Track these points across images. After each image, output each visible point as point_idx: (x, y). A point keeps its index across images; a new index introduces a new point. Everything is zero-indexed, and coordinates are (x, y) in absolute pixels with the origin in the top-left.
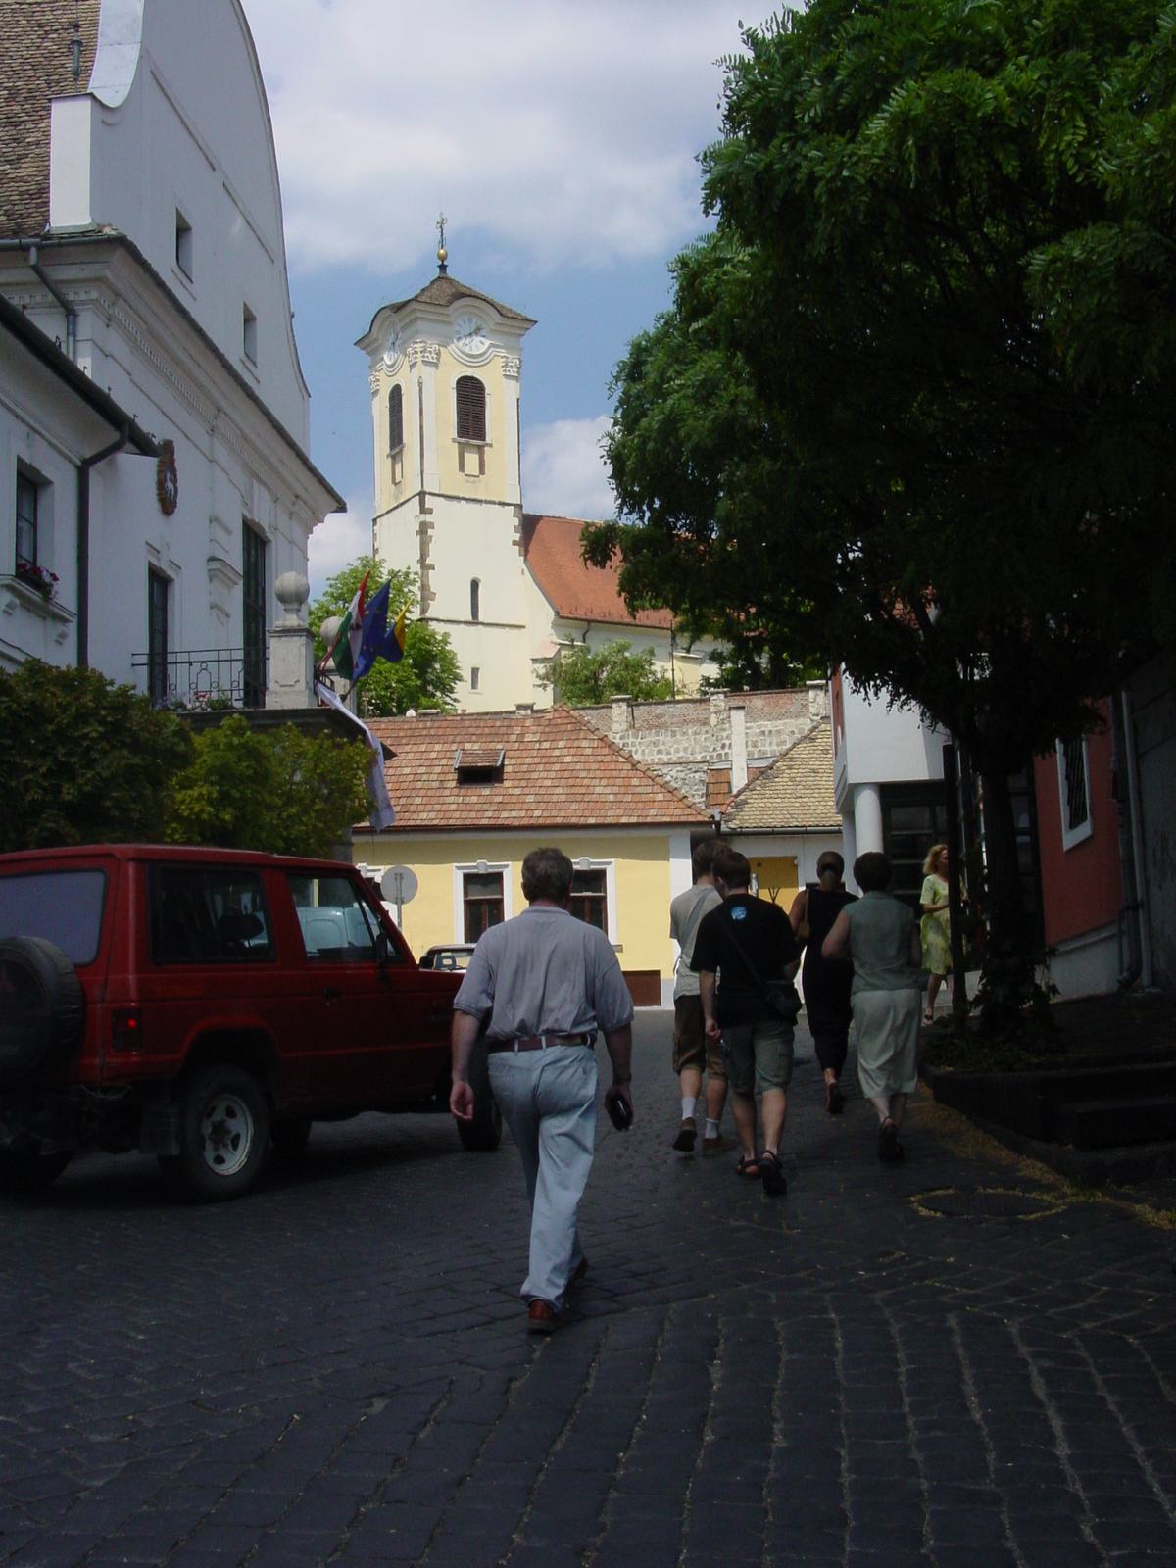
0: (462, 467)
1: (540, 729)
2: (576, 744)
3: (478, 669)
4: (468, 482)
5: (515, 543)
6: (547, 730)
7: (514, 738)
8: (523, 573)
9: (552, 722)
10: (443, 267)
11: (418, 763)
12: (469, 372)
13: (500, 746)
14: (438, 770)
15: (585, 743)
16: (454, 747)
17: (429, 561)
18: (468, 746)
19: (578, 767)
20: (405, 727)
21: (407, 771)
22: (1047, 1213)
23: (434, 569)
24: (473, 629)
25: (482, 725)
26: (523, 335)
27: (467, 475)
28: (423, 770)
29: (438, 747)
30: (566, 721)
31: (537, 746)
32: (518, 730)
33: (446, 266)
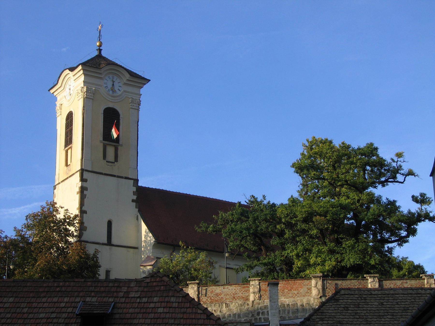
1: (141, 289)
2: (166, 299)
3: (109, 271)
4: (108, 165)
5: (133, 201)
6: (146, 289)
7: (121, 294)
9: (149, 284)
10: (100, 50)
11: (51, 310)
12: (111, 105)
13: (111, 300)
14: (65, 315)
15: (173, 299)
16: (78, 300)
18: (88, 299)
19: (168, 316)
20: (45, 285)
21: (42, 315)
24: (108, 247)
25: (99, 285)
26: (142, 87)
28: (54, 315)
29: (66, 300)
30: (160, 284)
31: (138, 300)
32: (125, 289)
33: (102, 50)
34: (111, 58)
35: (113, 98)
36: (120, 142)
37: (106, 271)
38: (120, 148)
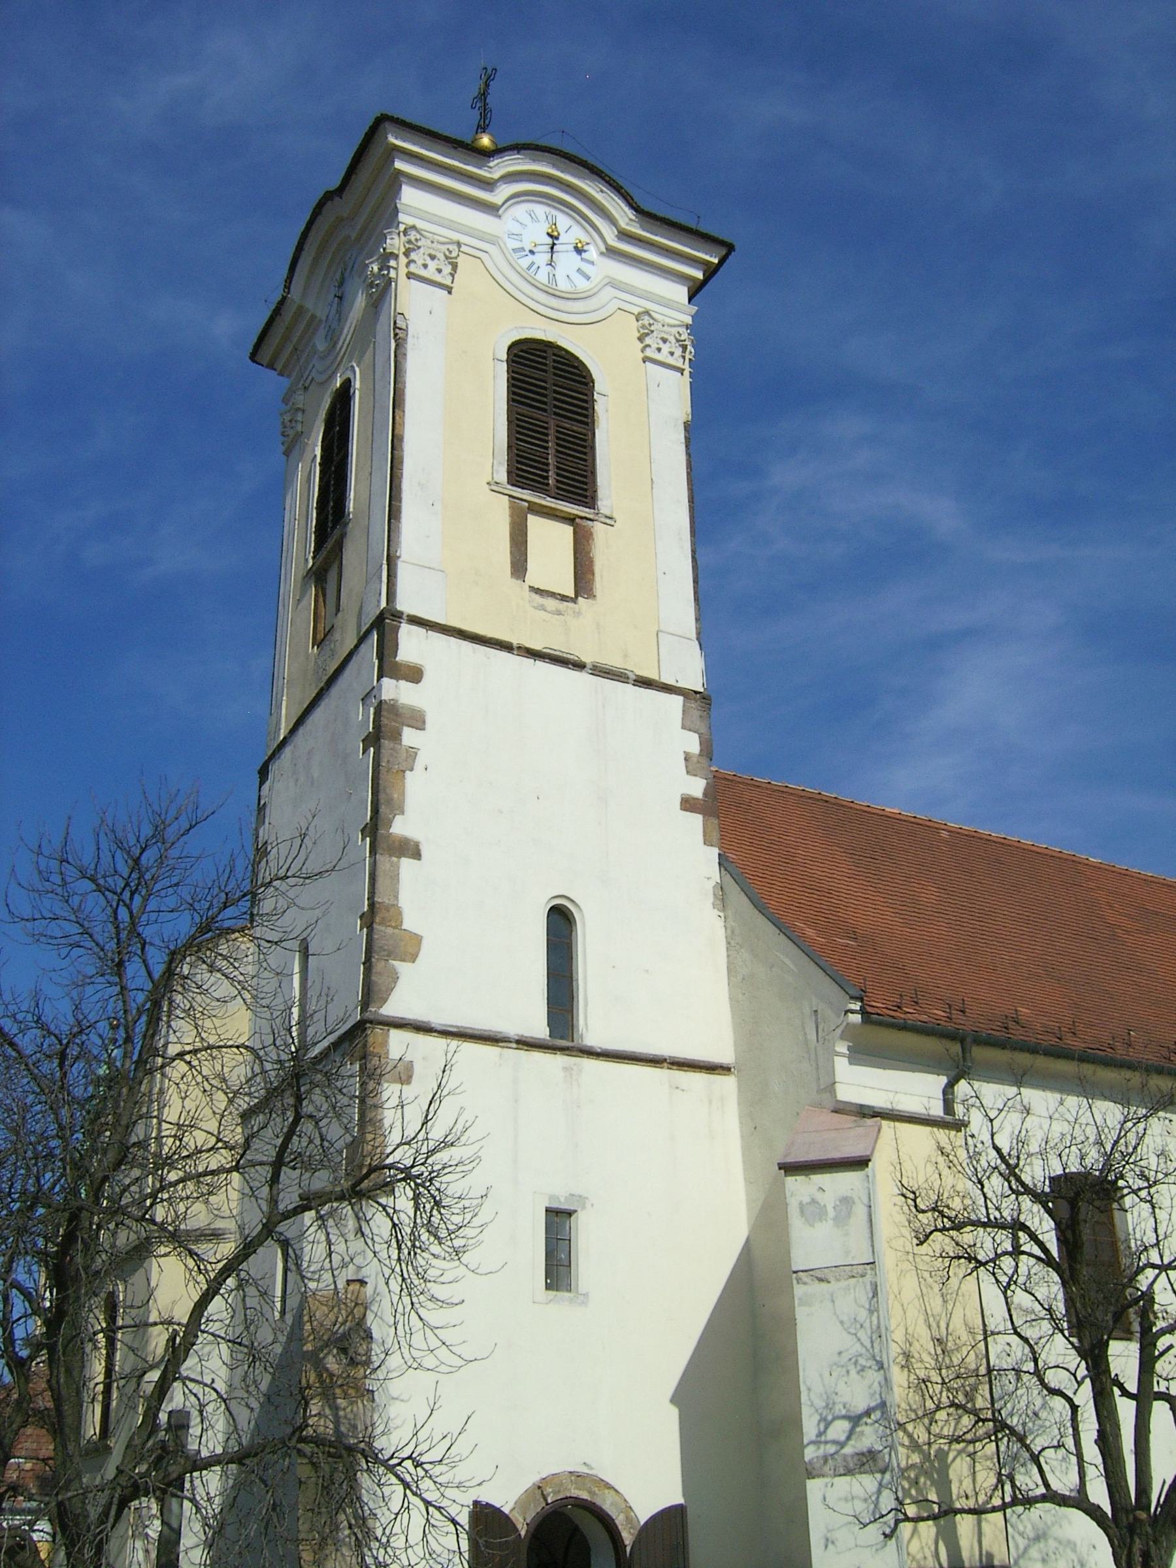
0: (519, 567)
4: (543, 608)
5: (688, 804)
8: (1096, 1564)
17: (400, 827)
22: (318, 460)
23: (417, 854)
24: (558, 1061)
27: (532, 589)
34: (692, 733)
35: (554, 302)
36: (599, 503)
37: (548, 1210)
38: (598, 529)
